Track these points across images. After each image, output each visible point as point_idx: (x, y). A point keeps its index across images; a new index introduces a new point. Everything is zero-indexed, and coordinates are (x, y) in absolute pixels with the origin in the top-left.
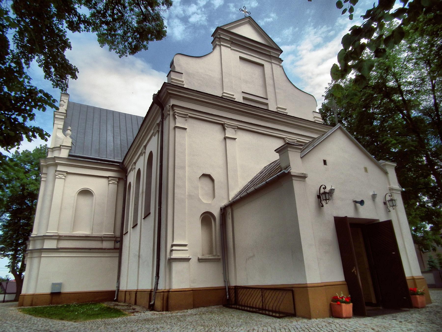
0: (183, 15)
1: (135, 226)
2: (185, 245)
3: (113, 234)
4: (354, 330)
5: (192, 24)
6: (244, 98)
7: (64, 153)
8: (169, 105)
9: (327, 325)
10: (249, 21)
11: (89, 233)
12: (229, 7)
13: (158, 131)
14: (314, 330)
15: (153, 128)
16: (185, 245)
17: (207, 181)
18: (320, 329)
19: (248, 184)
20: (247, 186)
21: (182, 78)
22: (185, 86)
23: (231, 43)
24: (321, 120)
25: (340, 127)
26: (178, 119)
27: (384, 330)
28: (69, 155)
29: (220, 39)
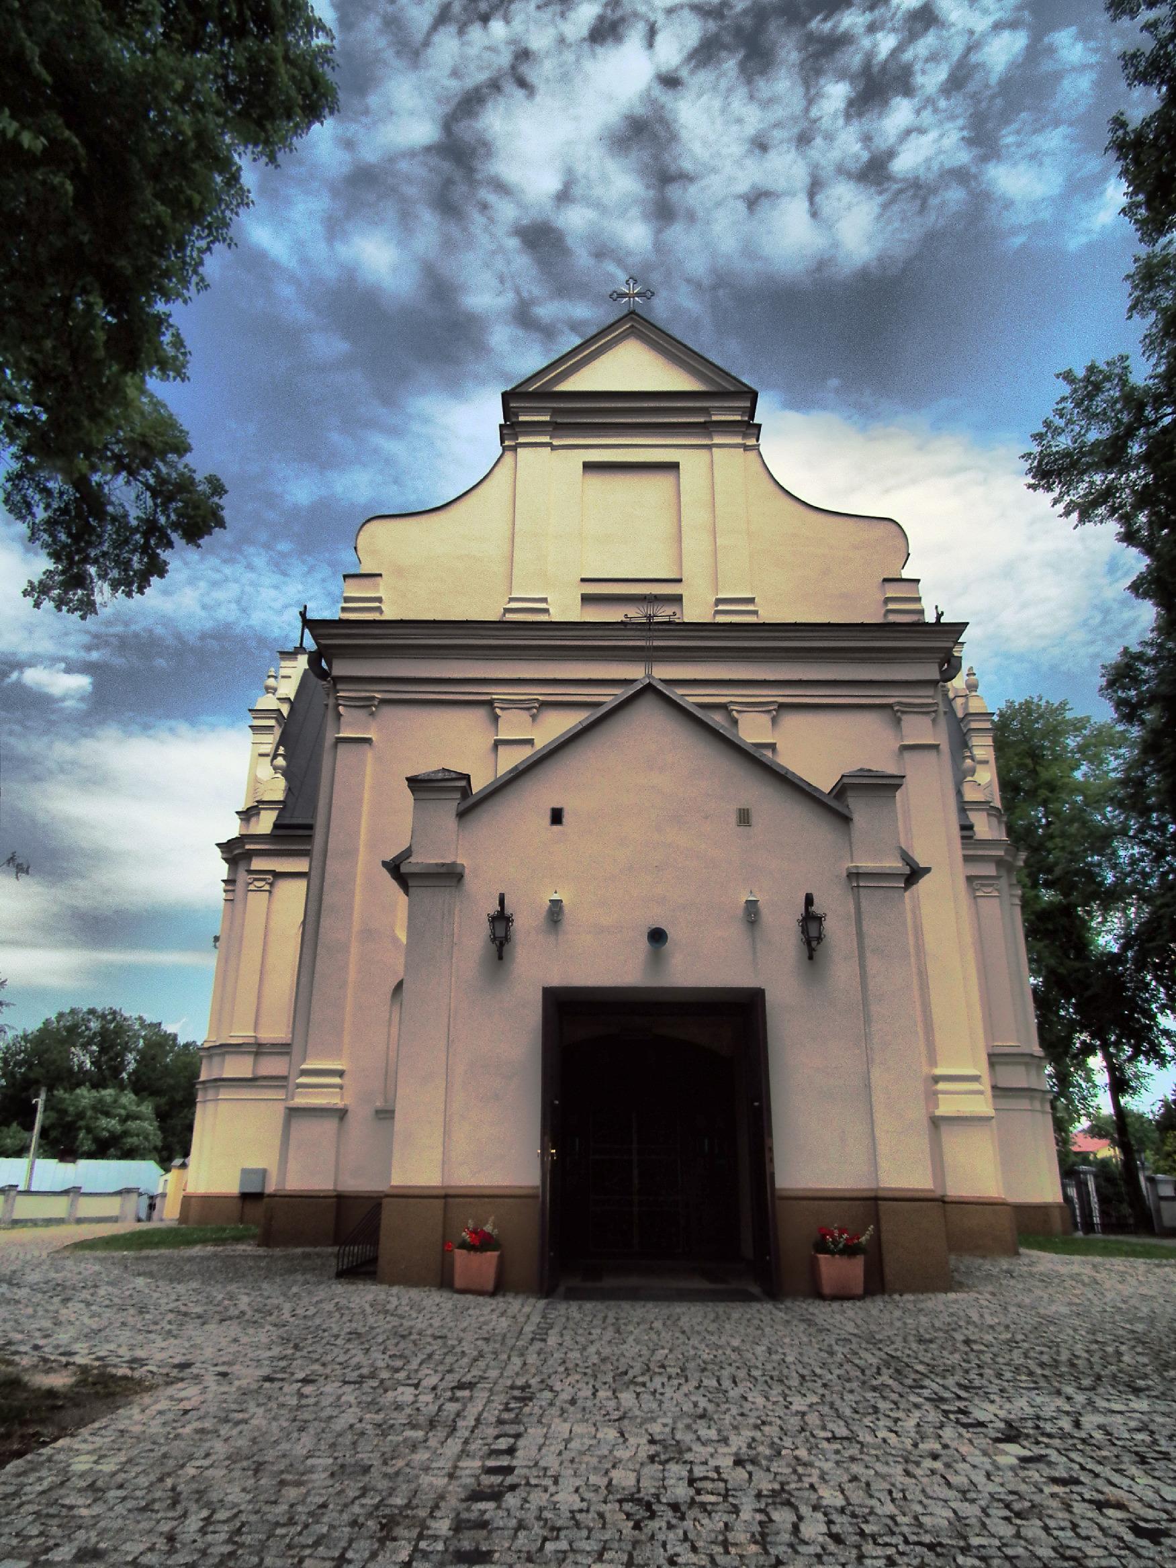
0: (865, 156)
5: (905, 180)
10: (632, 326)
12: (1051, 50)
23: (554, 429)
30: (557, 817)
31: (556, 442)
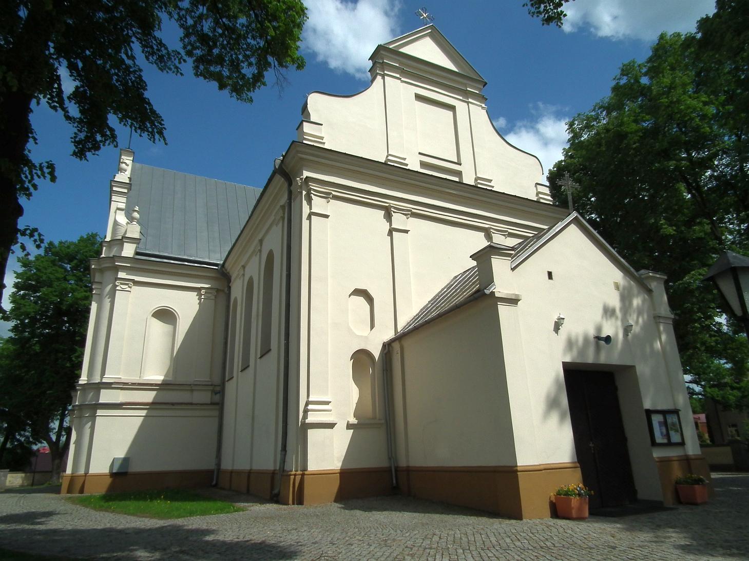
1: (245, 368)
2: (327, 403)
3: (209, 380)
4: (585, 536)
6: (423, 164)
7: (129, 250)
8: (302, 177)
9: (546, 529)
11: (171, 379)
13: (283, 218)
14: (524, 537)
15: (275, 211)
16: (327, 403)
17: (361, 300)
18: (533, 534)
19: (427, 304)
20: (426, 307)
21: (320, 131)
22: (326, 146)
24: (549, 198)
25: (576, 218)
26: (316, 200)
27: (630, 537)
28: (137, 253)
29: (383, 66)
30: (550, 275)
31: (403, 79)
